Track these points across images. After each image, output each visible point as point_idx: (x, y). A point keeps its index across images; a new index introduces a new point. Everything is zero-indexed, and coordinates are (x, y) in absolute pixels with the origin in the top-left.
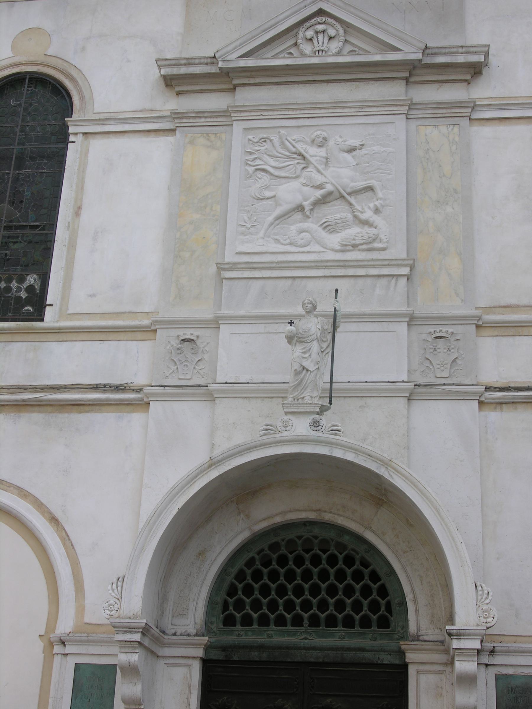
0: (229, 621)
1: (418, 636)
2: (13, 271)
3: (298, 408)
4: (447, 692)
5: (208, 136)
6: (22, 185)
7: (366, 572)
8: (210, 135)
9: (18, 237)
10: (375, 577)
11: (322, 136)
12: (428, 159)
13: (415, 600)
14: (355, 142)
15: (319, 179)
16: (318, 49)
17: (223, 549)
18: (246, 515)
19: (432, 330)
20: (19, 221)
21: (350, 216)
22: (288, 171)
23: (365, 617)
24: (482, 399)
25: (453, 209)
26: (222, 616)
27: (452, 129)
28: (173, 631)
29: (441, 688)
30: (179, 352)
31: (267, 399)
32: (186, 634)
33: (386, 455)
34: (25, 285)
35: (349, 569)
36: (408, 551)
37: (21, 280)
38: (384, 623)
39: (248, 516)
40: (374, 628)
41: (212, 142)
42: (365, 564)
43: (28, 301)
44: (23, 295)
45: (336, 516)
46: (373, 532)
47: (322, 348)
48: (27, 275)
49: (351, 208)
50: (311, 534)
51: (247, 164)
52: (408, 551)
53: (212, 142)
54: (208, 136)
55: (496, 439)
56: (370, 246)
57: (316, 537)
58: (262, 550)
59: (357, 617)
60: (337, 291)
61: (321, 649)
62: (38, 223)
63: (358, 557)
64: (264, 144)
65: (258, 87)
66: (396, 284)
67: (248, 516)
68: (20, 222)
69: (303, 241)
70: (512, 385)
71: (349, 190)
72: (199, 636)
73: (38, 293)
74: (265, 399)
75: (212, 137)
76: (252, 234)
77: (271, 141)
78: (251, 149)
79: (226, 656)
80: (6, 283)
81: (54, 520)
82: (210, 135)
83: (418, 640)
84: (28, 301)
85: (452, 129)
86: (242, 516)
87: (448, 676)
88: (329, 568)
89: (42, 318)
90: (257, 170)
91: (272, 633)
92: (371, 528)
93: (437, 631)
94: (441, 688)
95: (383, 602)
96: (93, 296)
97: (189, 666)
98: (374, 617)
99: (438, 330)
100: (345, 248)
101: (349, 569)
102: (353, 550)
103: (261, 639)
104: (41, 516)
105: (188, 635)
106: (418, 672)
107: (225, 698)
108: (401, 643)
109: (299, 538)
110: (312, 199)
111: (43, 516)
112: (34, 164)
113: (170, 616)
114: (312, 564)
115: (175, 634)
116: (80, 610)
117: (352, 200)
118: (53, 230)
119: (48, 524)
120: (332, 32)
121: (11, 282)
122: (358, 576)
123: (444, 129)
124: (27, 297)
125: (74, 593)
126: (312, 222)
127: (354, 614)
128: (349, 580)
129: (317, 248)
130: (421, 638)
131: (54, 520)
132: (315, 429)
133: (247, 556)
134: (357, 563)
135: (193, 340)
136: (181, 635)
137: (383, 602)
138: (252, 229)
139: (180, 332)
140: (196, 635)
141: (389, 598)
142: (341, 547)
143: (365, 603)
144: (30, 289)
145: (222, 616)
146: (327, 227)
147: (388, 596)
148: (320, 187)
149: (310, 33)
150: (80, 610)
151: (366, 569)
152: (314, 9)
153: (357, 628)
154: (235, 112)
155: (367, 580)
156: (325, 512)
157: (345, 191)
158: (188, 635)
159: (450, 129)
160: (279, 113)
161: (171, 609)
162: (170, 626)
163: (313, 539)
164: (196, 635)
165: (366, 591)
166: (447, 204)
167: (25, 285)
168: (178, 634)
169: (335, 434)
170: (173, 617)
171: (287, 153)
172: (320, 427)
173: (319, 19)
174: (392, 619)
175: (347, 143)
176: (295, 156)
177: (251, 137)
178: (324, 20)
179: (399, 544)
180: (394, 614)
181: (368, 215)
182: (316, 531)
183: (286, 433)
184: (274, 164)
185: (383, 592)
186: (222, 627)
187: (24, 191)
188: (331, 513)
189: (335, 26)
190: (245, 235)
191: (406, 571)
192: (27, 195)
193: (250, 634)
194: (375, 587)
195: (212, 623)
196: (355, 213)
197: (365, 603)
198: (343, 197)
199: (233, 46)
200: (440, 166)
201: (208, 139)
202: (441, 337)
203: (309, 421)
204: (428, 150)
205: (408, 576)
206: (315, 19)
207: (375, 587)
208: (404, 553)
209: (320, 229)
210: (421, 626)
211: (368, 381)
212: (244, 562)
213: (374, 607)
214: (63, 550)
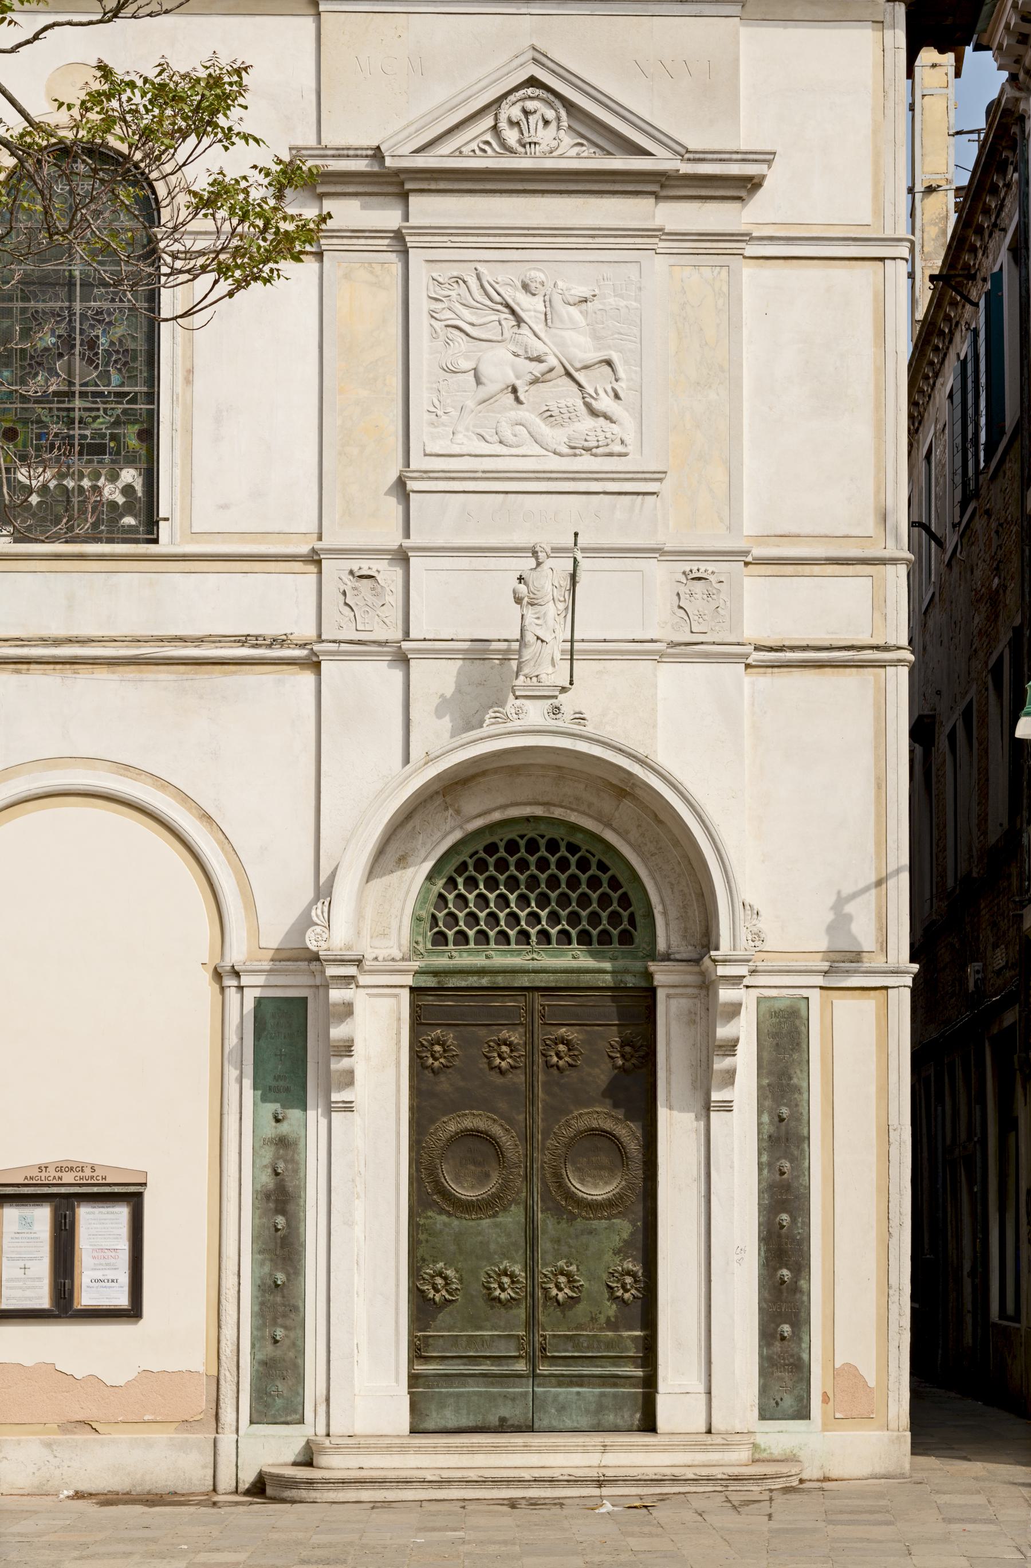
0: (440, 939)
1: (669, 955)
2: (98, 462)
3: (533, 690)
4: (701, 1018)
5: (371, 267)
6: (92, 327)
7: (605, 878)
8: (374, 265)
9: (98, 409)
10: (615, 884)
11: (539, 280)
12: (684, 319)
13: (665, 913)
14: (584, 291)
15: (537, 347)
16: (529, 140)
17: (429, 853)
18: (456, 811)
19: (688, 569)
20: (97, 385)
21: (580, 403)
22: (490, 331)
23: (605, 932)
24: (749, 661)
25: (718, 394)
26: (429, 934)
27: (719, 273)
28: (374, 956)
29: (695, 1014)
30: (356, 592)
31: (478, 661)
32: (390, 958)
33: (641, 751)
34: (120, 484)
35: (584, 874)
36: (656, 854)
37: (114, 477)
38: (626, 938)
39: (458, 812)
40: (616, 945)
41: (377, 276)
42: (603, 867)
43: (129, 508)
44: (121, 500)
45: (568, 811)
46: (614, 830)
47: (558, 609)
48: (121, 469)
49: (581, 391)
50: (537, 832)
51: (432, 317)
52: (656, 854)
53: (377, 276)
54: (371, 267)
55: (765, 713)
56: (607, 450)
57: (542, 837)
58: (476, 852)
59: (595, 933)
60: (576, 534)
61: (555, 972)
62: (126, 389)
63: (594, 861)
64: (455, 285)
65: (442, 194)
66: (642, 504)
67: (458, 812)
68: (99, 386)
69: (514, 438)
70: (787, 643)
71: (578, 365)
72: (406, 960)
73: (140, 498)
74: (475, 661)
75: (378, 268)
76: (445, 426)
77: (464, 282)
78: (437, 294)
79: (439, 982)
80: (90, 480)
81: (206, 818)
82: (374, 265)
83: (669, 960)
84: (129, 508)
85: (719, 273)
86: (450, 811)
87: (703, 1001)
88: (559, 874)
89: (155, 536)
90: (447, 326)
91: (493, 953)
92: (611, 825)
93: (690, 948)
94: (695, 1014)
95: (625, 914)
96: (225, 507)
97: (396, 996)
98: (615, 932)
99: (695, 569)
100: (574, 450)
101: (584, 874)
102: (587, 851)
103: (479, 961)
104: (188, 813)
105: (393, 960)
106: (668, 996)
107: (439, 1031)
108: (650, 964)
109: (522, 837)
110: (529, 378)
111: (191, 813)
112: (107, 293)
113: (369, 937)
114: (537, 868)
115: (376, 959)
116: (255, 931)
117: (579, 376)
118: (153, 404)
119: (198, 823)
120: (550, 114)
121: (98, 479)
122: (594, 883)
123: (706, 272)
124: (125, 502)
125: (243, 910)
126: (528, 410)
127: (590, 929)
128: (584, 888)
129: (538, 450)
130: (672, 957)
131: (206, 818)
132: (554, 717)
133: (488, 840)
134: (594, 867)
135: (373, 577)
136: (384, 960)
137: (625, 914)
138: (444, 417)
139: (354, 565)
140: (403, 959)
141: (631, 909)
142: (573, 848)
143: (604, 915)
144: (128, 490)
145: (429, 934)
146: (548, 416)
147: (630, 905)
148: (539, 360)
149: (516, 113)
150: (255, 931)
151: (605, 873)
152: (524, 77)
153: (595, 946)
154: (411, 235)
155: (605, 888)
156: (555, 805)
157: (572, 365)
158: (393, 960)
159: (715, 273)
160: (475, 239)
161: (369, 927)
162: (370, 950)
163: (539, 839)
164: (403, 959)
165: (604, 901)
166: (710, 387)
167: (120, 484)
168: (380, 959)
169: (579, 724)
170: (372, 937)
171: (489, 303)
172: (560, 715)
173: (530, 91)
174: (636, 933)
175: (573, 292)
176: (500, 307)
177: (435, 275)
178: (536, 94)
179: (646, 844)
180: (638, 928)
181: (604, 403)
182: (543, 828)
183: (518, 723)
184: (473, 319)
185: (625, 901)
186: (431, 947)
187: (97, 337)
188: (562, 807)
189: (553, 104)
190: (436, 427)
191: (654, 878)
192: (103, 344)
193: (465, 954)
194: (615, 896)
195: (417, 943)
196: (587, 399)
197: (604, 915)
198: (568, 374)
199: (406, 133)
200: (701, 330)
201: (372, 272)
202: (700, 579)
203: (547, 707)
204: (685, 303)
205: (656, 884)
206: (524, 91)
207: (615, 896)
208: (652, 855)
209: (538, 421)
210: (672, 942)
211: (608, 638)
212: (453, 868)
213: (615, 919)
214: (222, 857)
